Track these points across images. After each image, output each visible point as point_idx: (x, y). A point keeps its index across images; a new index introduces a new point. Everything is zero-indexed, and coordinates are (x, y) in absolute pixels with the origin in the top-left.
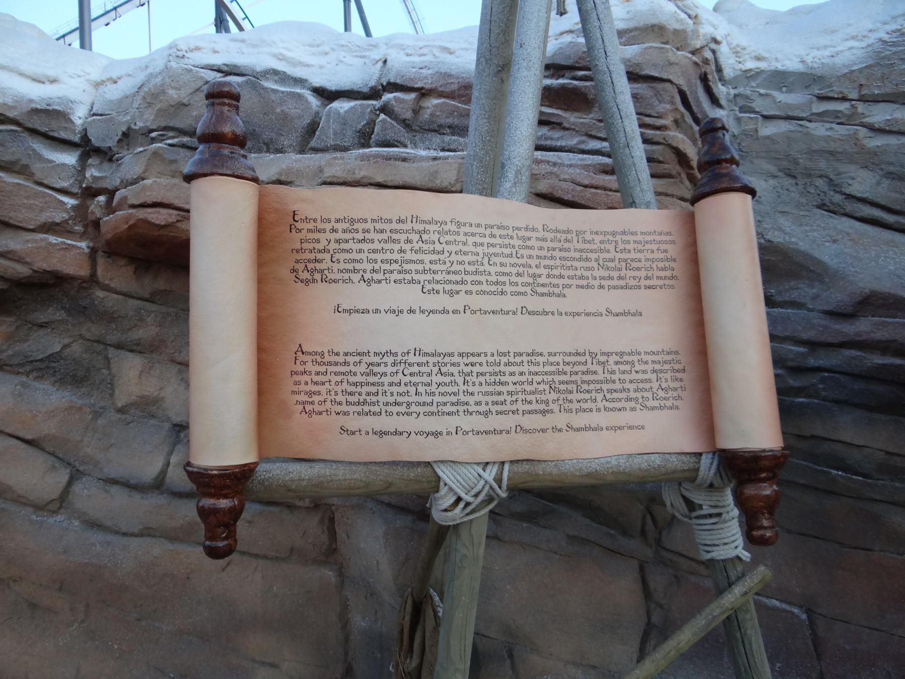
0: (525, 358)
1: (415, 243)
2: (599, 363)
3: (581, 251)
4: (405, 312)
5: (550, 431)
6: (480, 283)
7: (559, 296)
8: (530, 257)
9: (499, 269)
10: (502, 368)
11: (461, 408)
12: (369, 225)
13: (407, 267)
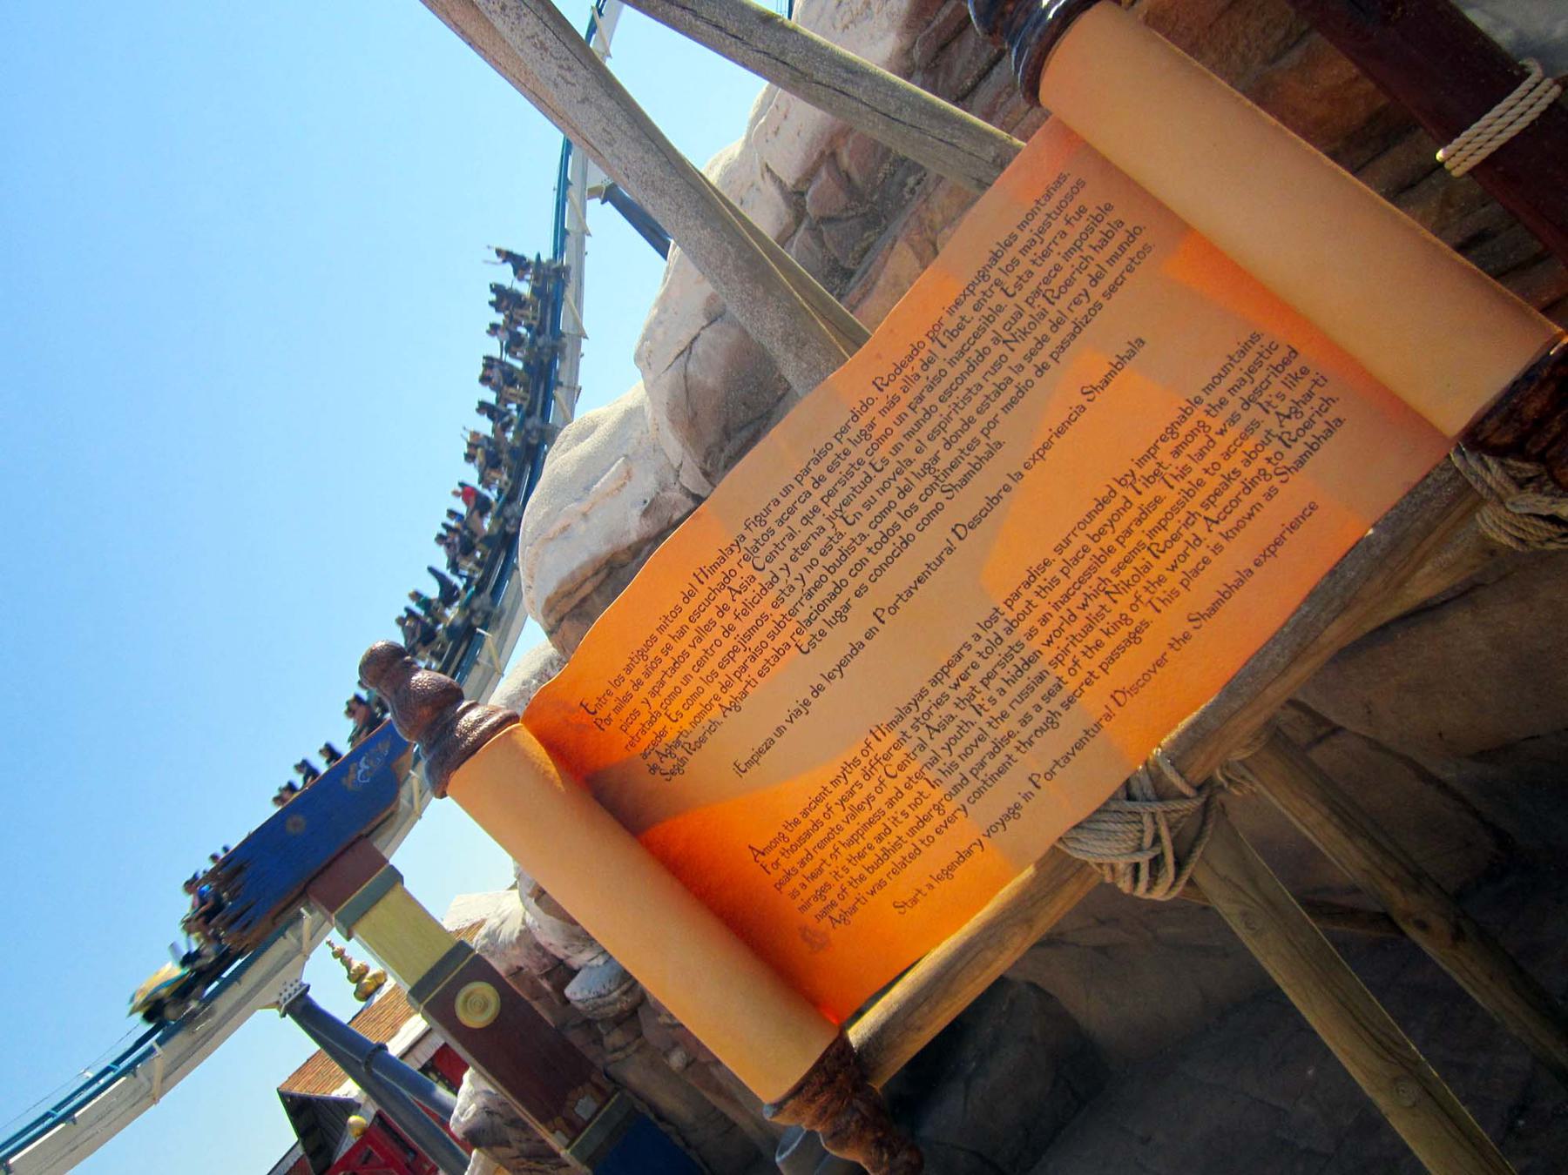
0: (1027, 594)
1: (731, 604)
2: (1148, 481)
3: (962, 352)
4: (811, 699)
5: (1171, 654)
6: (863, 563)
7: (990, 454)
8: (897, 449)
9: (869, 516)
10: (1010, 640)
11: (1009, 749)
12: (663, 639)
13: (753, 644)
